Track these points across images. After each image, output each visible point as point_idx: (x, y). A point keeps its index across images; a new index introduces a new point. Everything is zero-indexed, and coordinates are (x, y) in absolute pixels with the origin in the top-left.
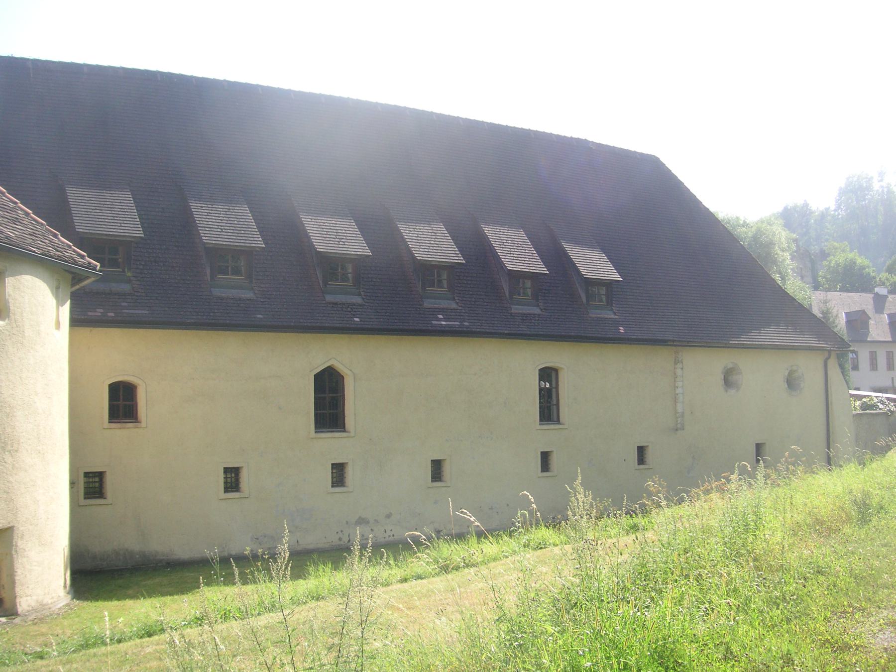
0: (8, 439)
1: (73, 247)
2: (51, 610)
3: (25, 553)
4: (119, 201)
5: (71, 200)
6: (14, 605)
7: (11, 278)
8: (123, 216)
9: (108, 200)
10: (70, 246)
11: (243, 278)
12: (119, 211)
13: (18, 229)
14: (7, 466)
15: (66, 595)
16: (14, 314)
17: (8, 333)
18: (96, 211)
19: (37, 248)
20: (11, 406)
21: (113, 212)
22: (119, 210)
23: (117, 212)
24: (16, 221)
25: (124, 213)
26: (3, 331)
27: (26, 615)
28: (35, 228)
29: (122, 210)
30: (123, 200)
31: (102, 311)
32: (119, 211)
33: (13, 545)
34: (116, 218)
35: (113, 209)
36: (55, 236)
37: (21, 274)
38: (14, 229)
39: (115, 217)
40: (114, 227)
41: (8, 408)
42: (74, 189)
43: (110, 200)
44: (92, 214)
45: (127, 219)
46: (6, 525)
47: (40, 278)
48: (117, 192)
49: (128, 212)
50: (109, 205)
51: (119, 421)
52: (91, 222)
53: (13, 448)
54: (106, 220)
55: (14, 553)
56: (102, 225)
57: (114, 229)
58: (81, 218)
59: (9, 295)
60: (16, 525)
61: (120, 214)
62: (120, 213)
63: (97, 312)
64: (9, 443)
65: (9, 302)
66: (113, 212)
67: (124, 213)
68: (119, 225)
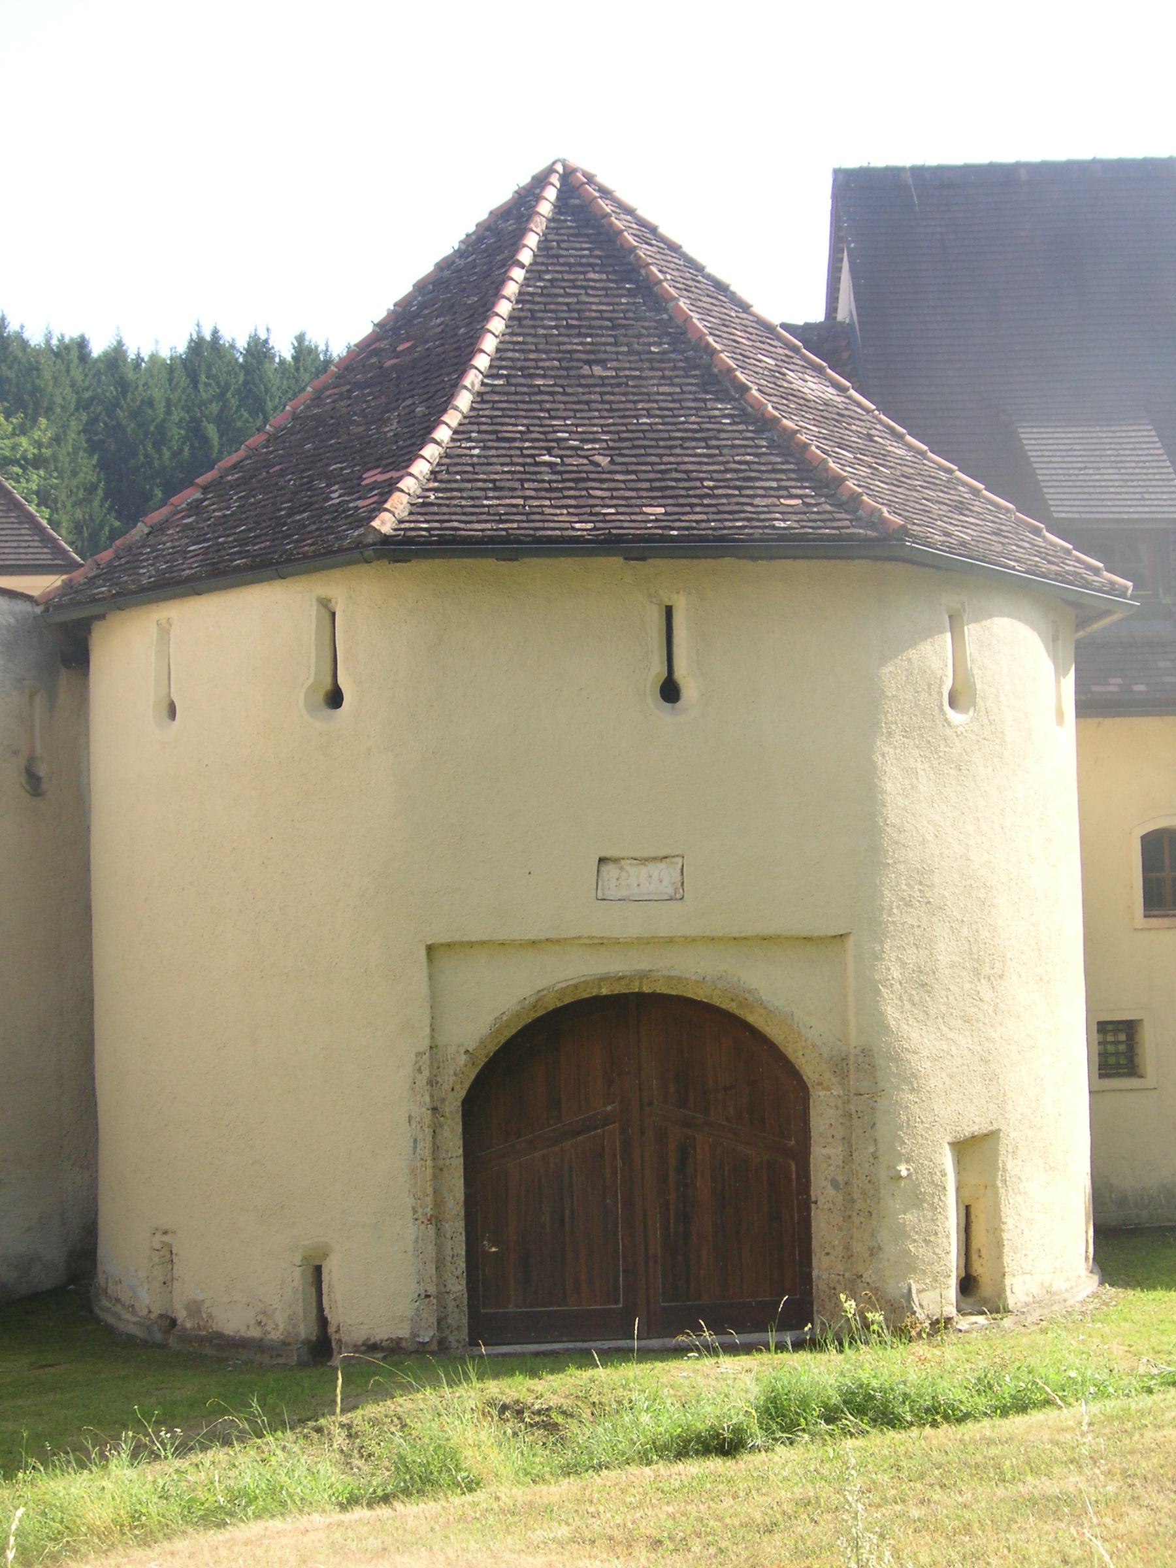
0: (985, 952)
1: (1075, 552)
2: (1067, 1304)
3: (1021, 1186)
4: (1131, 446)
5: (1034, 454)
6: (1000, 1293)
7: (974, 625)
8: (1144, 477)
9: (1108, 447)
10: (1068, 552)
11: (1150, 593)
12: (1134, 468)
13: (972, 524)
14: (985, 1007)
15: (1090, 1275)
16: (984, 698)
17: (974, 738)
18: (1087, 471)
19: (1016, 561)
20: (988, 884)
21: (1123, 471)
22: (1134, 465)
23: (1131, 471)
24: (961, 507)
25: (1145, 471)
26: (965, 734)
27: (1023, 1313)
28: (997, 520)
29: (1140, 465)
30: (1141, 443)
31: (1119, 681)
32: (1134, 468)
33: (998, 1169)
34: (1130, 483)
35: (1122, 465)
36: (1036, 531)
37: (991, 616)
38: (965, 526)
39: (1128, 481)
40: (1129, 503)
41: (982, 890)
42: (1035, 430)
43: (1113, 446)
44: (1081, 478)
45: (1154, 483)
46: (986, 1128)
47: (1026, 622)
48: (1124, 428)
49: (1153, 468)
50: (1110, 456)
51: (1163, 912)
52: (1080, 496)
53: (995, 970)
54: (1112, 490)
55: (1000, 1185)
56: (1103, 500)
57: (1130, 506)
58: (1059, 490)
59: (972, 661)
60: (1003, 1128)
61: (1137, 474)
62: (1137, 471)
63: (1109, 684)
64: (987, 960)
65: (973, 675)
66: (1123, 471)
67: (1145, 471)
68: (1138, 496)
